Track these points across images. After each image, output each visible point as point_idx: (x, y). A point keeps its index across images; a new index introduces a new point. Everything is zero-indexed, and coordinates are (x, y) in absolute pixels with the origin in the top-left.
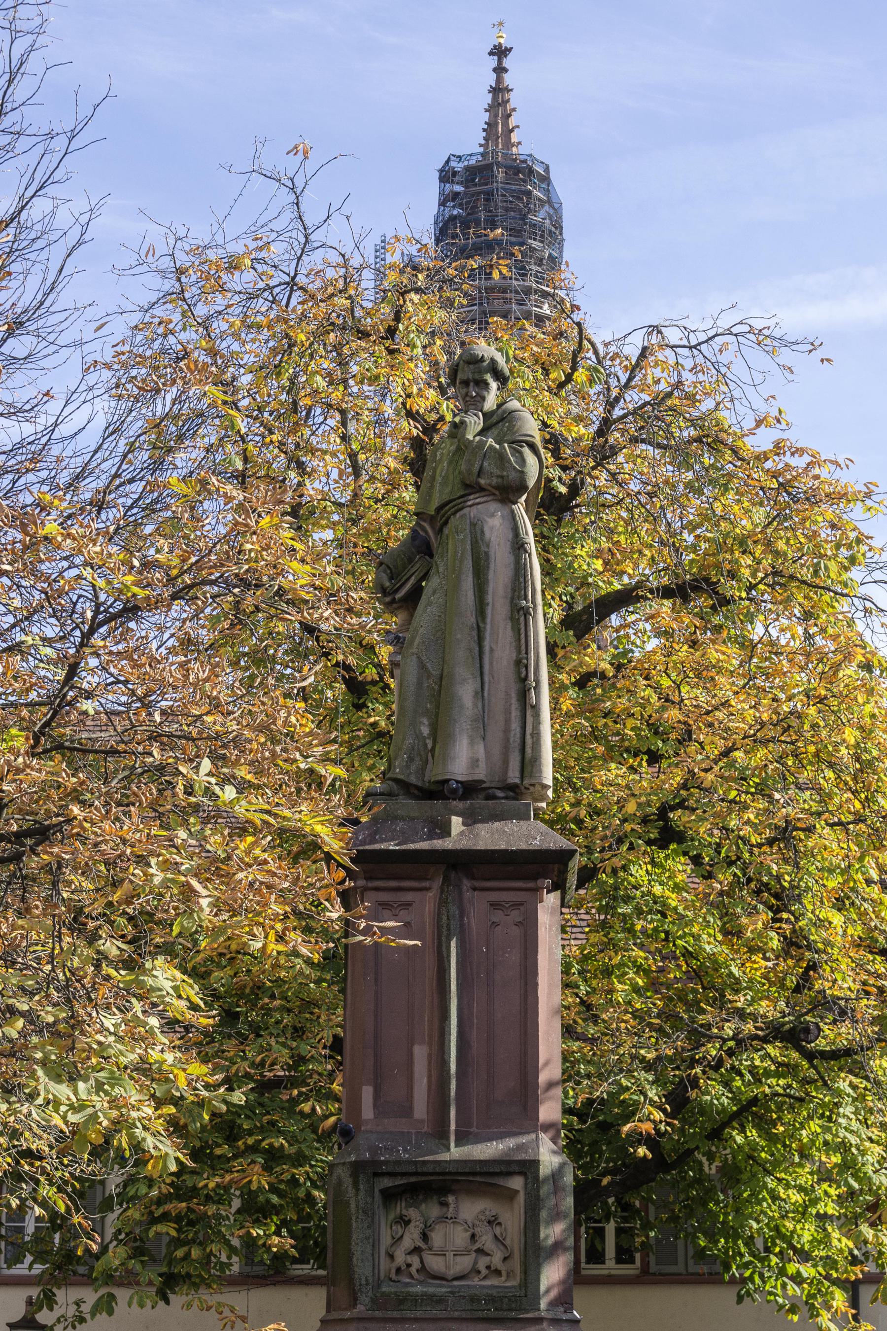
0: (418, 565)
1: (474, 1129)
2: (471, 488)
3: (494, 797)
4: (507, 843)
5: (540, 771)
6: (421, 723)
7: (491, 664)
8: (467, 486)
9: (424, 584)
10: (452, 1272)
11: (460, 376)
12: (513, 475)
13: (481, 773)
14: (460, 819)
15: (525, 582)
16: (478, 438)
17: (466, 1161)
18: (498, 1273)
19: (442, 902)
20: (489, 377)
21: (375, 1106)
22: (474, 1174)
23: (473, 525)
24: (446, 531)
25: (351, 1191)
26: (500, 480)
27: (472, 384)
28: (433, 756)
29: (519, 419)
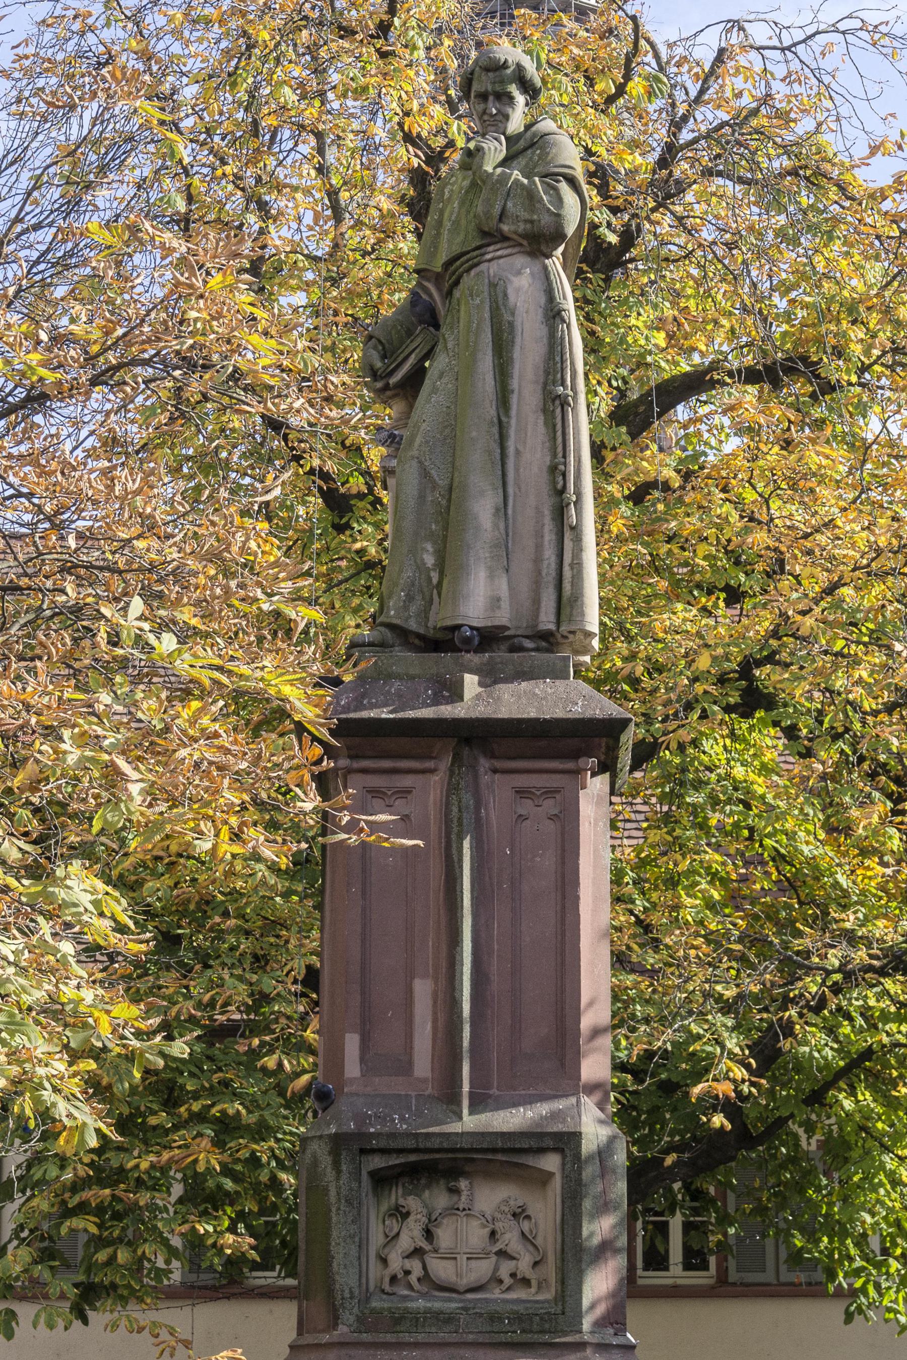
0: (419, 340)
1: (494, 1091)
2: (490, 236)
3: (521, 649)
4: (539, 709)
5: (583, 614)
7: (517, 470)
8: (484, 234)
9: (427, 364)
10: (465, 1281)
11: (476, 87)
12: (546, 220)
13: (503, 617)
14: (476, 678)
15: (563, 361)
16: (499, 170)
17: (483, 1134)
18: (526, 1282)
19: (452, 789)
20: (514, 89)
21: (362, 1060)
22: (495, 1151)
23: (493, 286)
24: (457, 293)
25: (330, 1174)
26: (528, 226)
27: (491, 98)
28: (439, 594)
29: (555, 144)
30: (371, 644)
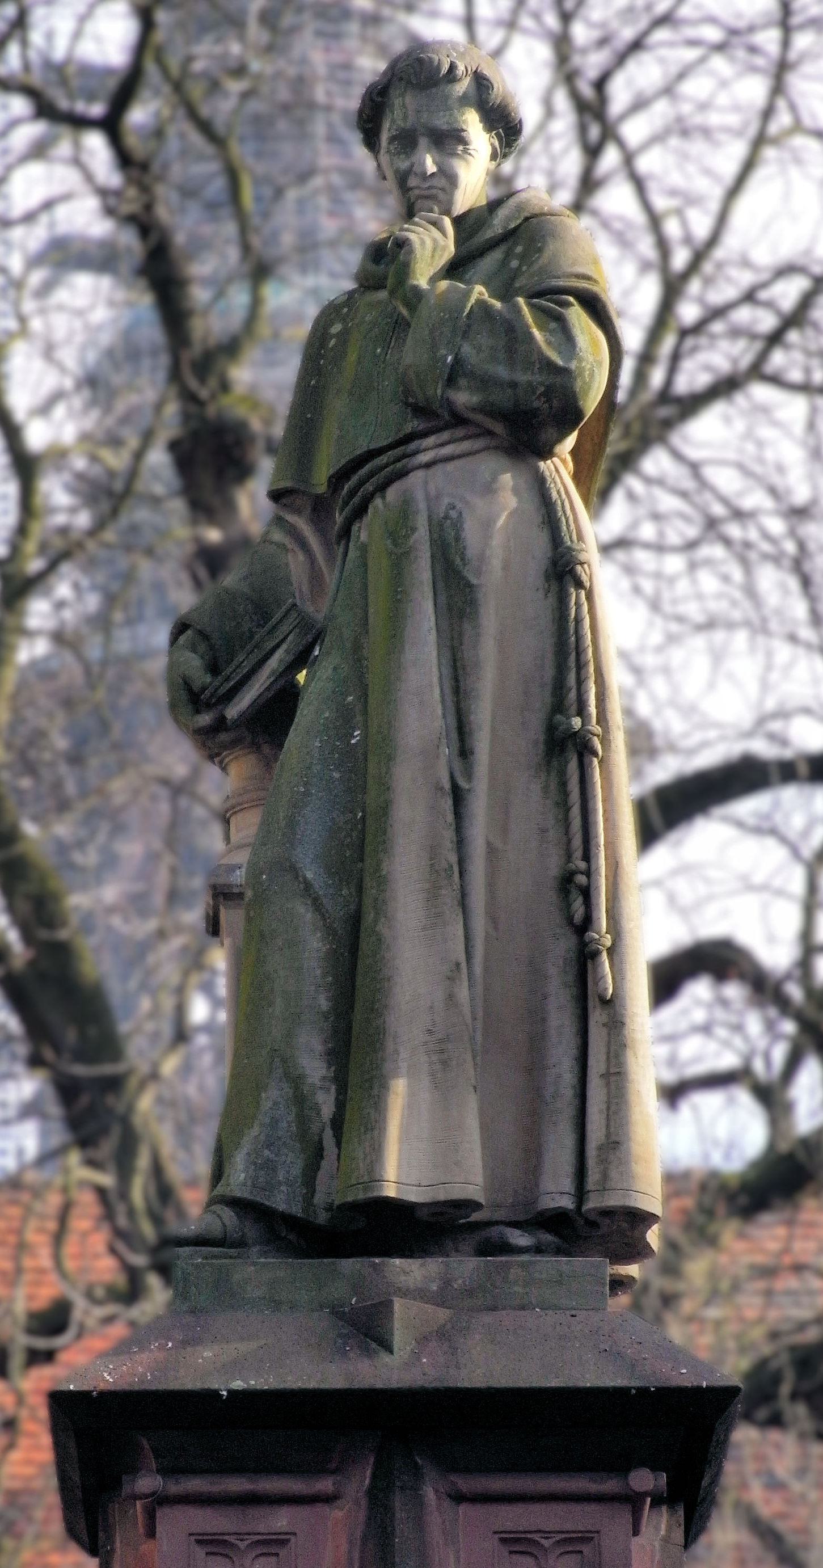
2: (432, 416)
3: (506, 1248)
9: (301, 677)
13: (470, 1180)
20: (472, 123)
27: (423, 142)
30: (200, 1241)
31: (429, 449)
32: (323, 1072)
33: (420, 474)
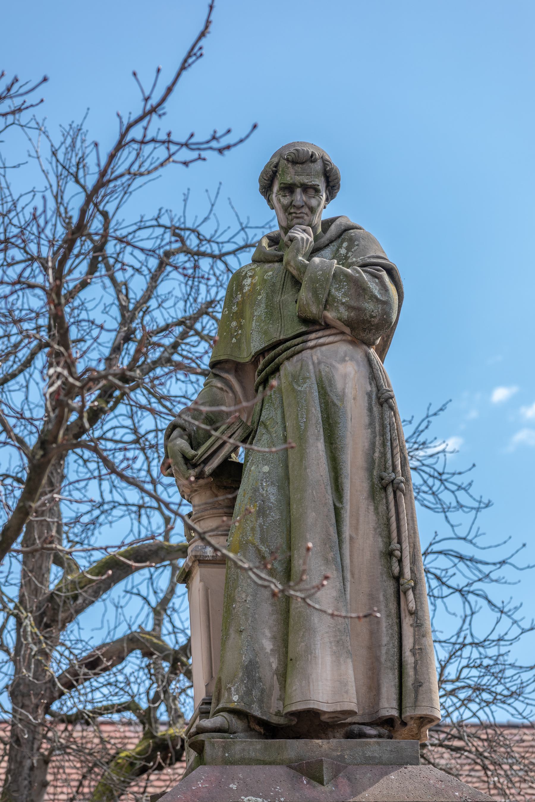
2: (311, 323)
3: (362, 735)
6: (263, 634)
8: (305, 321)
13: (350, 701)
27: (299, 190)
31: (313, 339)
32: (272, 647)
33: (309, 351)
